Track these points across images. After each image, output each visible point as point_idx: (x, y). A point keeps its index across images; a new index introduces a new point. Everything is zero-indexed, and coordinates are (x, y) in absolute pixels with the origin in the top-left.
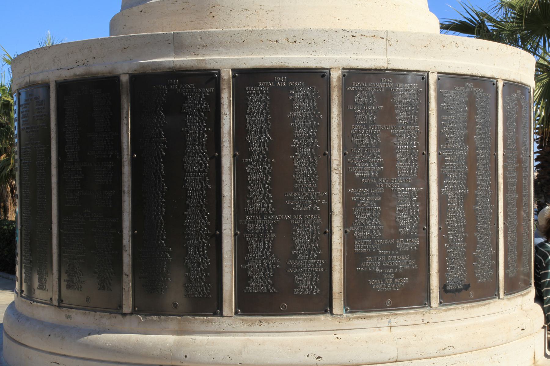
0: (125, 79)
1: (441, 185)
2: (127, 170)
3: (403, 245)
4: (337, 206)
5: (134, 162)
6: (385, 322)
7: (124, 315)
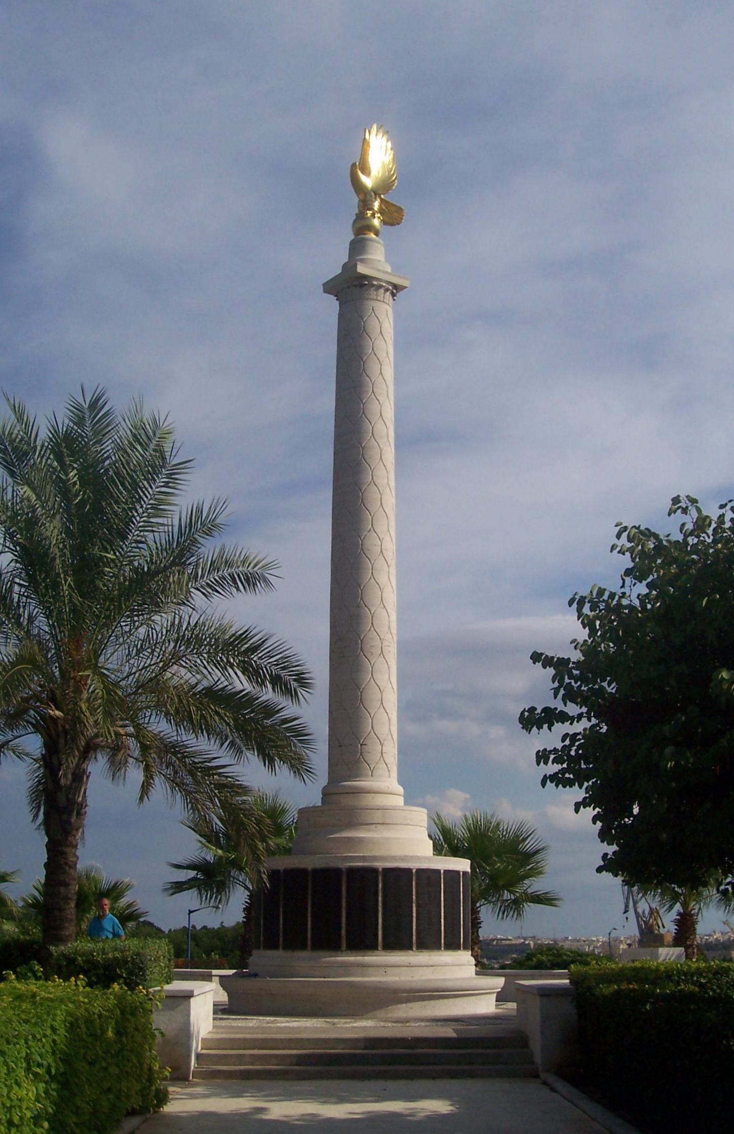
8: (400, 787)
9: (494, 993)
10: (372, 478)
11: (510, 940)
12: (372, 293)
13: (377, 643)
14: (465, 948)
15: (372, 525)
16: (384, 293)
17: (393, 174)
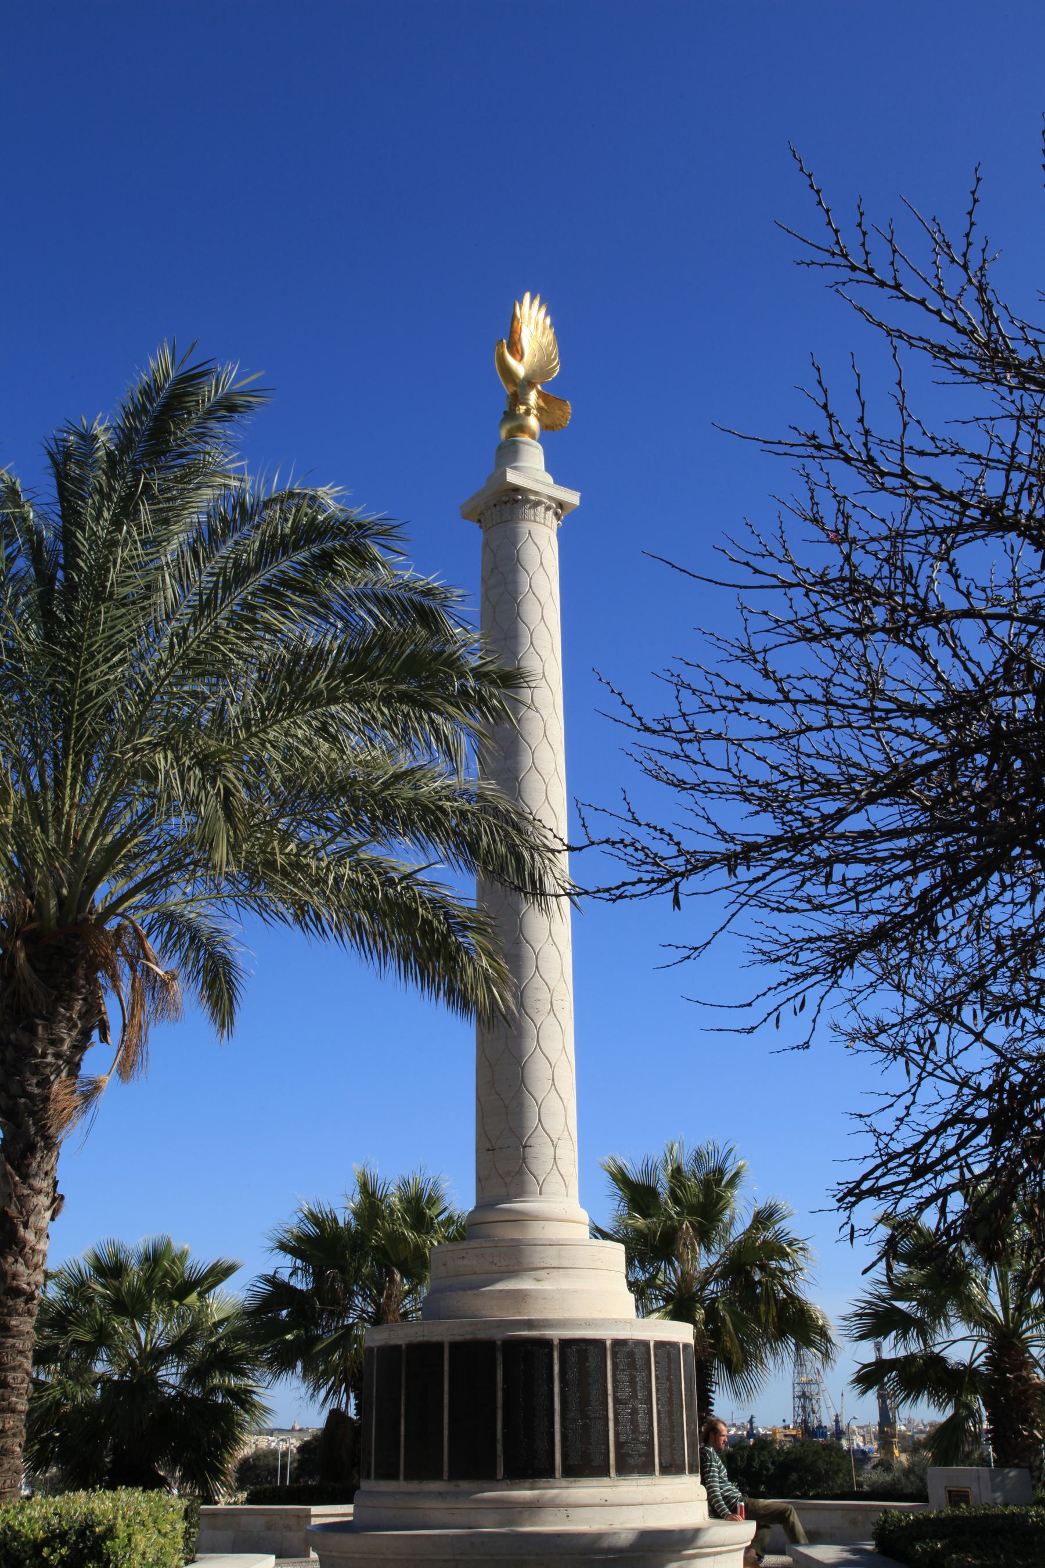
0: (499, 1343)
1: (658, 1405)
2: (500, 1395)
3: (642, 1438)
4: (611, 1415)
5: (504, 1390)
6: (634, 1483)
7: (498, 1481)
13: (545, 995)
16: (545, 513)
17: (554, 360)
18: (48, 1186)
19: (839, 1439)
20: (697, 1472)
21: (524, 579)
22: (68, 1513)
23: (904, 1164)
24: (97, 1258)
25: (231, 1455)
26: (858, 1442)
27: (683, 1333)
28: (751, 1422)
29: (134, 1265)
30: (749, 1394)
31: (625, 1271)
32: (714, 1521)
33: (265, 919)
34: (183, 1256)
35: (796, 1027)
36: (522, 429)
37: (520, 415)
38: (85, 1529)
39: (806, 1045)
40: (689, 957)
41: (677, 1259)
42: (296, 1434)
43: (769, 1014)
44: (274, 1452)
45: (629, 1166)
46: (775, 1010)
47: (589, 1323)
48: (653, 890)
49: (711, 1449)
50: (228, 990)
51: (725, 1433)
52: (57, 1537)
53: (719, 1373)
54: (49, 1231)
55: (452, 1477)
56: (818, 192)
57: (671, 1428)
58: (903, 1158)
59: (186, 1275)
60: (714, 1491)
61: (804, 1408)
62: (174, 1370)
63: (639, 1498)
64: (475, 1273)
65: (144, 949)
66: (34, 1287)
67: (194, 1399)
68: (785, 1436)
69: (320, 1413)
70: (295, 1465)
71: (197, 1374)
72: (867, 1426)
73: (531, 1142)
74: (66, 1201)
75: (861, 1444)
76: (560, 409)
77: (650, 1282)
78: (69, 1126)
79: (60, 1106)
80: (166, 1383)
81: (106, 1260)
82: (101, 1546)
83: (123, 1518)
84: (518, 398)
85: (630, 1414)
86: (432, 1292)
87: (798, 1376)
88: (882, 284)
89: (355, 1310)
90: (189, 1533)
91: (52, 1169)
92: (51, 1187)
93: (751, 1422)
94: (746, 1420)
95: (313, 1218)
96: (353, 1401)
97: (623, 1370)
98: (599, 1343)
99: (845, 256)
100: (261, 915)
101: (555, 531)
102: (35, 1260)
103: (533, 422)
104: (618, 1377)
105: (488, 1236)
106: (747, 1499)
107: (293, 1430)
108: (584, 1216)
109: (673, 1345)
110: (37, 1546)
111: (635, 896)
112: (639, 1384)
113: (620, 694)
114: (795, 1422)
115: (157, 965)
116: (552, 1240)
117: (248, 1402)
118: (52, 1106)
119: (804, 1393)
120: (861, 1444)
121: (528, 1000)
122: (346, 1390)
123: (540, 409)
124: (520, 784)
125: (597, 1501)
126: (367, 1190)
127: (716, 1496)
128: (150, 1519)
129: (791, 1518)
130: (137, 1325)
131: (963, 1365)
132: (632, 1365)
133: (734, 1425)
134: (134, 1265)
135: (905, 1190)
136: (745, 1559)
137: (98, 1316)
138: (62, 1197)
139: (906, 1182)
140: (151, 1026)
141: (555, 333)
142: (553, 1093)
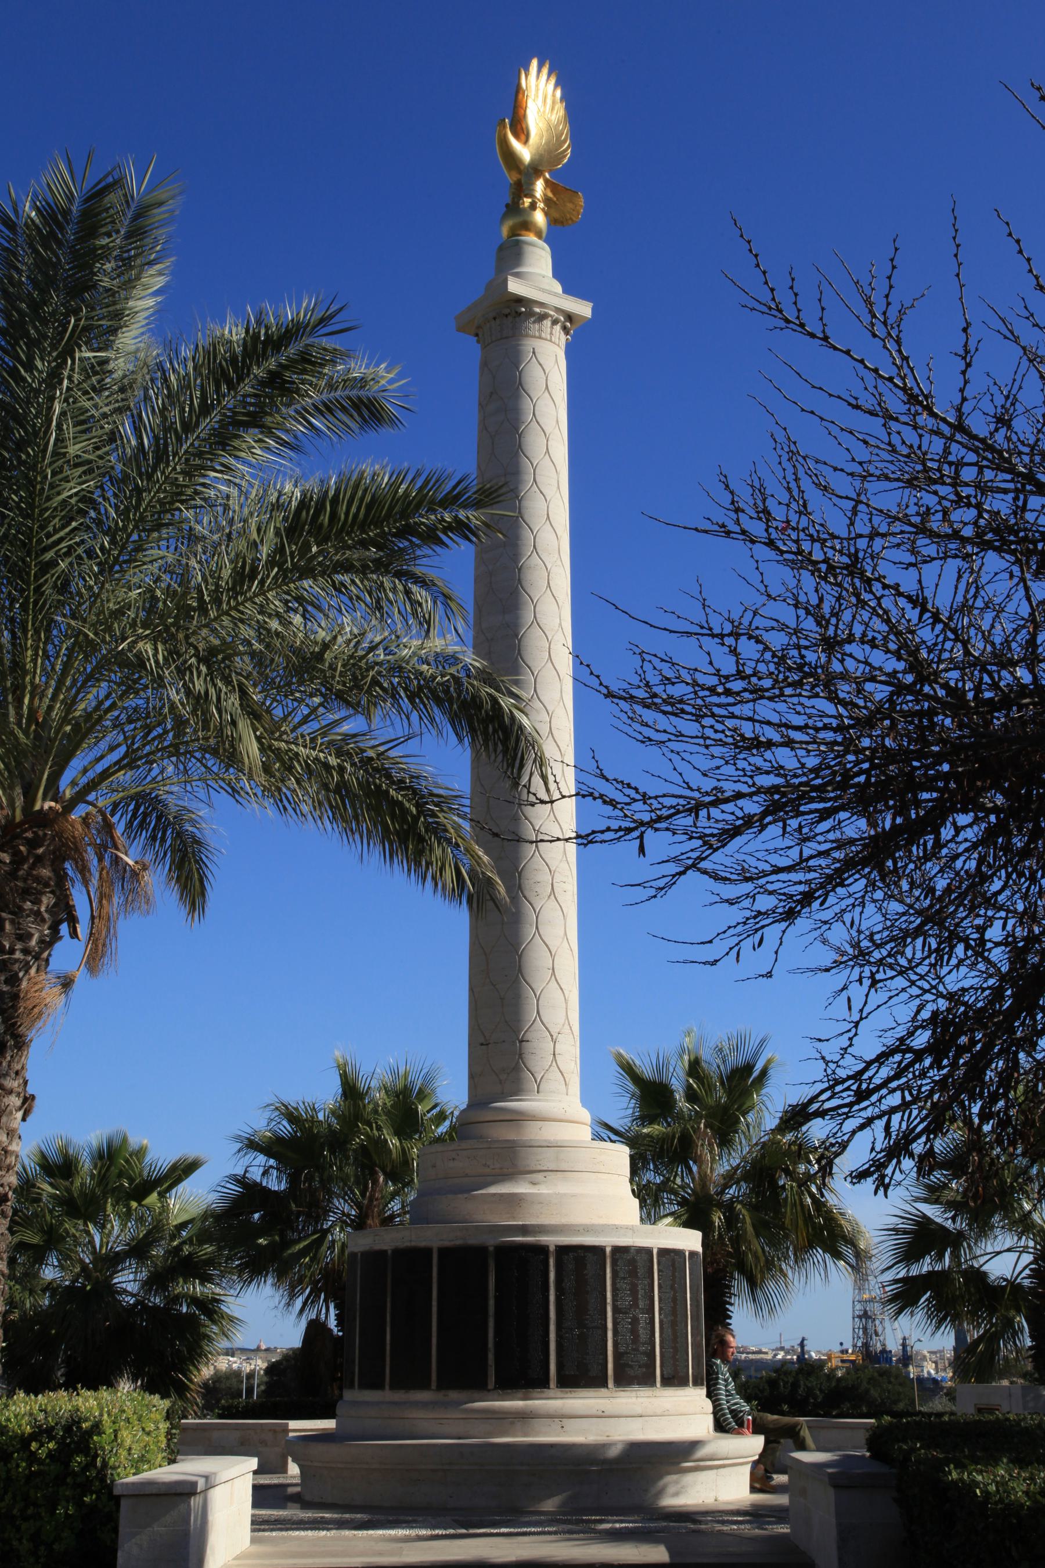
0: (491, 1249)
1: (660, 1314)
2: (492, 1302)
4: (610, 1325)
5: (496, 1298)
6: (634, 1394)
7: (489, 1391)
8: (585, 1110)
9: (746, 1463)
10: (535, 617)
11: (766, 1353)
12: (534, 328)
13: (545, 877)
14: (696, 1383)
15: (535, 690)
16: (552, 328)
17: (565, 141)
18: (19, 1085)
19: (906, 1366)
20: (702, 1385)
21: (527, 405)
22: (53, 1409)
23: (848, 1089)
24: (43, 1156)
25: (199, 1370)
26: (929, 1369)
27: (691, 1240)
28: (802, 1344)
29: (86, 1164)
30: (771, 1310)
31: (629, 1175)
32: (719, 1434)
33: (237, 801)
34: (140, 1153)
35: (756, 960)
36: (527, 225)
37: (524, 209)
38: (73, 1423)
39: (769, 975)
40: (655, 896)
41: (695, 1162)
42: (262, 1354)
43: (731, 949)
44: (237, 1374)
45: (638, 1062)
46: (737, 945)
47: (588, 1229)
48: (621, 837)
49: (719, 1362)
50: (198, 870)
51: (733, 1345)
52: (42, 1433)
53: (739, 1284)
54: (20, 1132)
55: (441, 1387)
56: (756, 256)
57: (675, 1339)
58: (846, 1085)
59: (145, 1173)
60: (720, 1405)
61: (865, 1329)
62: (131, 1277)
63: (639, 1410)
64: (467, 1176)
65: (112, 838)
66: (7, 1188)
67: (156, 1307)
68: (843, 1361)
69: (296, 1325)
70: (263, 1388)
71: (157, 1281)
72: (940, 1351)
73: (529, 1036)
74: (37, 1102)
75: (933, 1372)
76: (571, 201)
77: (663, 1187)
78: (39, 1024)
79: (30, 1004)
80: (125, 1291)
81: (54, 1157)
82: (88, 1441)
83: (109, 1415)
84: (522, 188)
85: (630, 1323)
86: (421, 1194)
87: (859, 1293)
88: (813, 336)
89: (335, 1213)
90: (171, 1434)
91: (23, 1068)
92: (22, 1087)
93: (802, 1344)
94: (796, 1343)
95: (291, 1116)
96: (333, 1312)
97: (624, 1278)
98: (599, 1250)
99: (781, 311)
100: (234, 797)
101: (563, 347)
102: (8, 1161)
103: (539, 218)
104: (618, 1286)
105: (481, 1137)
106: (756, 1413)
107: (258, 1349)
108: (586, 1116)
109: (679, 1253)
110: (24, 1441)
111: (605, 841)
112: (641, 1293)
113: (588, 666)
114: (854, 1346)
115: (126, 855)
116: (549, 1141)
117: (215, 1312)
118: (22, 1004)
119: (866, 1312)
120: (933, 1372)
121: (526, 882)
122: (326, 1301)
123: (547, 201)
124: (520, 641)
125: (594, 1412)
126: (351, 1090)
127: (722, 1409)
128: (135, 1417)
129: (802, 1433)
130: (91, 1227)
131: (1005, 1280)
132: (633, 1273)
133: (782, 1349)
134: (86, 1164)
135: (849, 1112)
136: (752, 1474)
137: (48, 1218)
138: (33, 1097)
139: (850, 1105)
140: (121, 917)
141: (567, 108)
142: (553, 983)
